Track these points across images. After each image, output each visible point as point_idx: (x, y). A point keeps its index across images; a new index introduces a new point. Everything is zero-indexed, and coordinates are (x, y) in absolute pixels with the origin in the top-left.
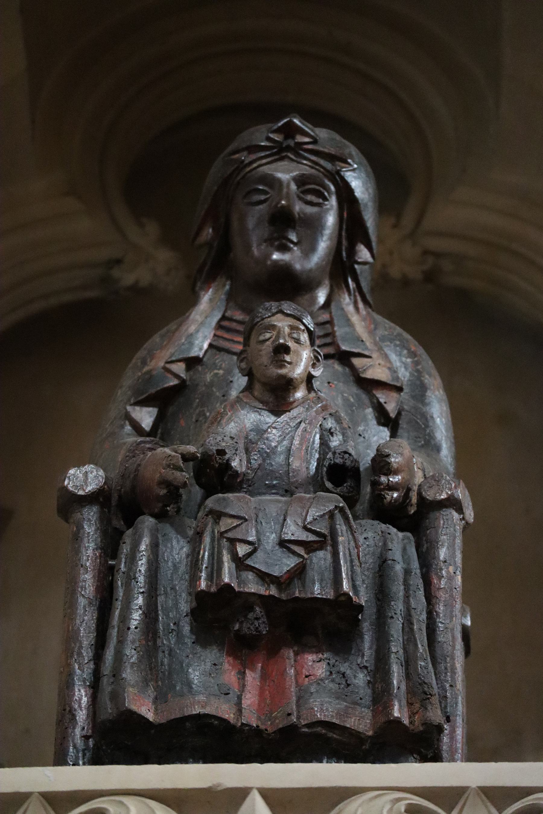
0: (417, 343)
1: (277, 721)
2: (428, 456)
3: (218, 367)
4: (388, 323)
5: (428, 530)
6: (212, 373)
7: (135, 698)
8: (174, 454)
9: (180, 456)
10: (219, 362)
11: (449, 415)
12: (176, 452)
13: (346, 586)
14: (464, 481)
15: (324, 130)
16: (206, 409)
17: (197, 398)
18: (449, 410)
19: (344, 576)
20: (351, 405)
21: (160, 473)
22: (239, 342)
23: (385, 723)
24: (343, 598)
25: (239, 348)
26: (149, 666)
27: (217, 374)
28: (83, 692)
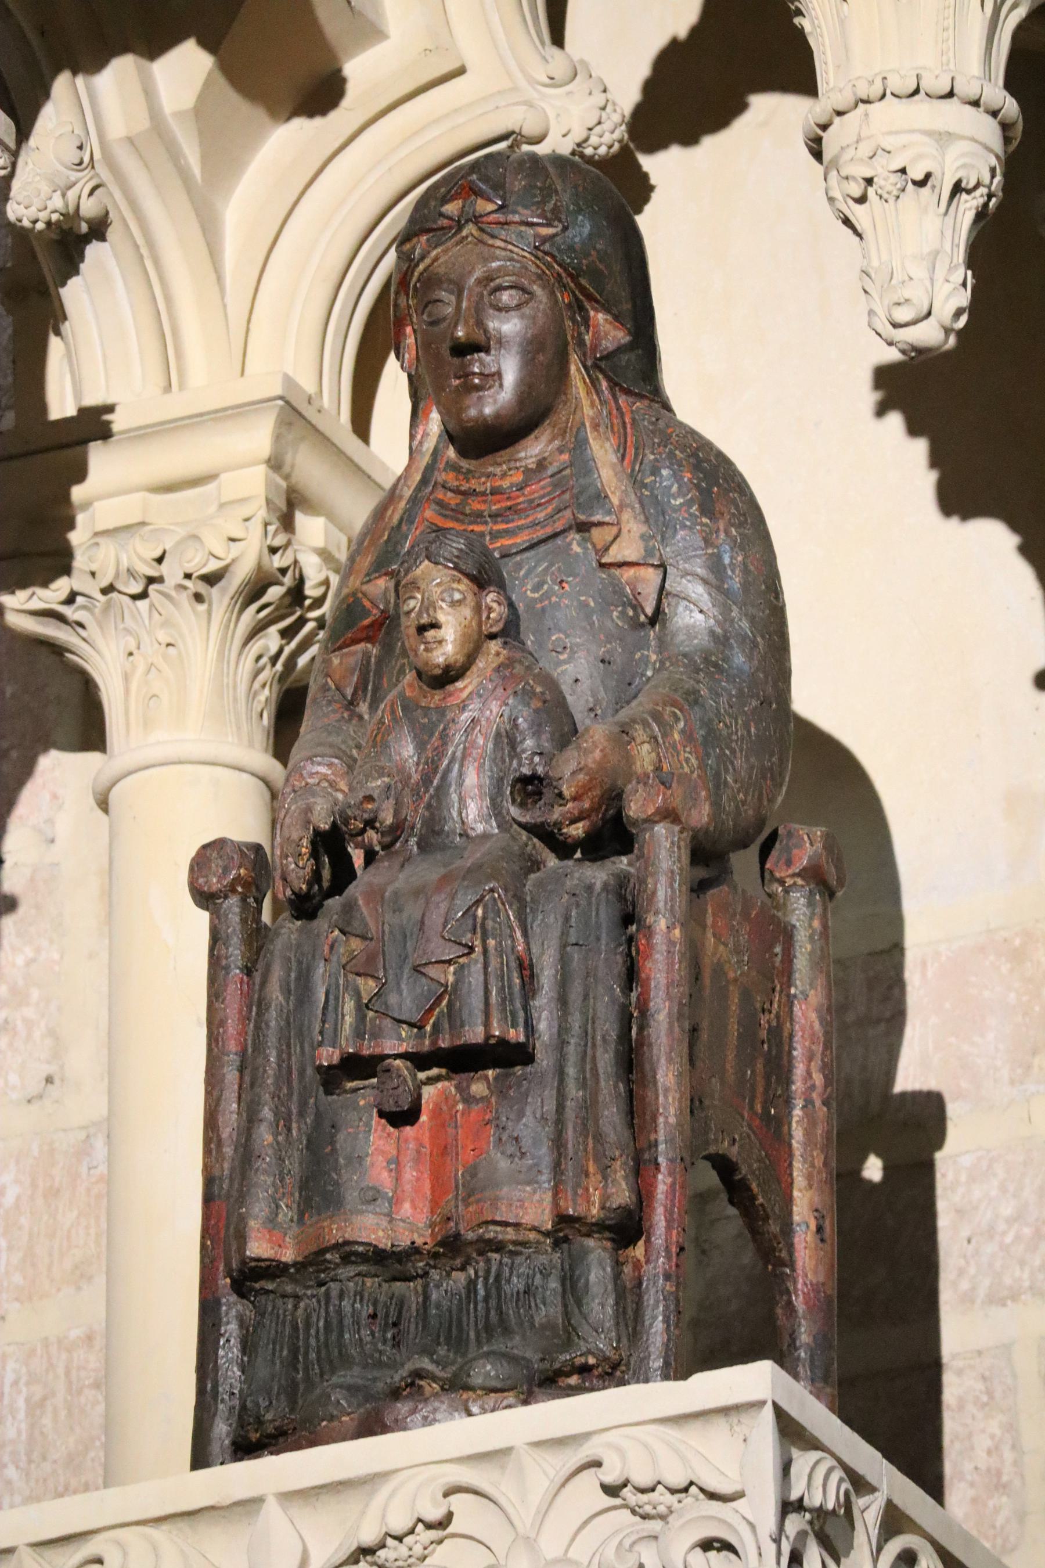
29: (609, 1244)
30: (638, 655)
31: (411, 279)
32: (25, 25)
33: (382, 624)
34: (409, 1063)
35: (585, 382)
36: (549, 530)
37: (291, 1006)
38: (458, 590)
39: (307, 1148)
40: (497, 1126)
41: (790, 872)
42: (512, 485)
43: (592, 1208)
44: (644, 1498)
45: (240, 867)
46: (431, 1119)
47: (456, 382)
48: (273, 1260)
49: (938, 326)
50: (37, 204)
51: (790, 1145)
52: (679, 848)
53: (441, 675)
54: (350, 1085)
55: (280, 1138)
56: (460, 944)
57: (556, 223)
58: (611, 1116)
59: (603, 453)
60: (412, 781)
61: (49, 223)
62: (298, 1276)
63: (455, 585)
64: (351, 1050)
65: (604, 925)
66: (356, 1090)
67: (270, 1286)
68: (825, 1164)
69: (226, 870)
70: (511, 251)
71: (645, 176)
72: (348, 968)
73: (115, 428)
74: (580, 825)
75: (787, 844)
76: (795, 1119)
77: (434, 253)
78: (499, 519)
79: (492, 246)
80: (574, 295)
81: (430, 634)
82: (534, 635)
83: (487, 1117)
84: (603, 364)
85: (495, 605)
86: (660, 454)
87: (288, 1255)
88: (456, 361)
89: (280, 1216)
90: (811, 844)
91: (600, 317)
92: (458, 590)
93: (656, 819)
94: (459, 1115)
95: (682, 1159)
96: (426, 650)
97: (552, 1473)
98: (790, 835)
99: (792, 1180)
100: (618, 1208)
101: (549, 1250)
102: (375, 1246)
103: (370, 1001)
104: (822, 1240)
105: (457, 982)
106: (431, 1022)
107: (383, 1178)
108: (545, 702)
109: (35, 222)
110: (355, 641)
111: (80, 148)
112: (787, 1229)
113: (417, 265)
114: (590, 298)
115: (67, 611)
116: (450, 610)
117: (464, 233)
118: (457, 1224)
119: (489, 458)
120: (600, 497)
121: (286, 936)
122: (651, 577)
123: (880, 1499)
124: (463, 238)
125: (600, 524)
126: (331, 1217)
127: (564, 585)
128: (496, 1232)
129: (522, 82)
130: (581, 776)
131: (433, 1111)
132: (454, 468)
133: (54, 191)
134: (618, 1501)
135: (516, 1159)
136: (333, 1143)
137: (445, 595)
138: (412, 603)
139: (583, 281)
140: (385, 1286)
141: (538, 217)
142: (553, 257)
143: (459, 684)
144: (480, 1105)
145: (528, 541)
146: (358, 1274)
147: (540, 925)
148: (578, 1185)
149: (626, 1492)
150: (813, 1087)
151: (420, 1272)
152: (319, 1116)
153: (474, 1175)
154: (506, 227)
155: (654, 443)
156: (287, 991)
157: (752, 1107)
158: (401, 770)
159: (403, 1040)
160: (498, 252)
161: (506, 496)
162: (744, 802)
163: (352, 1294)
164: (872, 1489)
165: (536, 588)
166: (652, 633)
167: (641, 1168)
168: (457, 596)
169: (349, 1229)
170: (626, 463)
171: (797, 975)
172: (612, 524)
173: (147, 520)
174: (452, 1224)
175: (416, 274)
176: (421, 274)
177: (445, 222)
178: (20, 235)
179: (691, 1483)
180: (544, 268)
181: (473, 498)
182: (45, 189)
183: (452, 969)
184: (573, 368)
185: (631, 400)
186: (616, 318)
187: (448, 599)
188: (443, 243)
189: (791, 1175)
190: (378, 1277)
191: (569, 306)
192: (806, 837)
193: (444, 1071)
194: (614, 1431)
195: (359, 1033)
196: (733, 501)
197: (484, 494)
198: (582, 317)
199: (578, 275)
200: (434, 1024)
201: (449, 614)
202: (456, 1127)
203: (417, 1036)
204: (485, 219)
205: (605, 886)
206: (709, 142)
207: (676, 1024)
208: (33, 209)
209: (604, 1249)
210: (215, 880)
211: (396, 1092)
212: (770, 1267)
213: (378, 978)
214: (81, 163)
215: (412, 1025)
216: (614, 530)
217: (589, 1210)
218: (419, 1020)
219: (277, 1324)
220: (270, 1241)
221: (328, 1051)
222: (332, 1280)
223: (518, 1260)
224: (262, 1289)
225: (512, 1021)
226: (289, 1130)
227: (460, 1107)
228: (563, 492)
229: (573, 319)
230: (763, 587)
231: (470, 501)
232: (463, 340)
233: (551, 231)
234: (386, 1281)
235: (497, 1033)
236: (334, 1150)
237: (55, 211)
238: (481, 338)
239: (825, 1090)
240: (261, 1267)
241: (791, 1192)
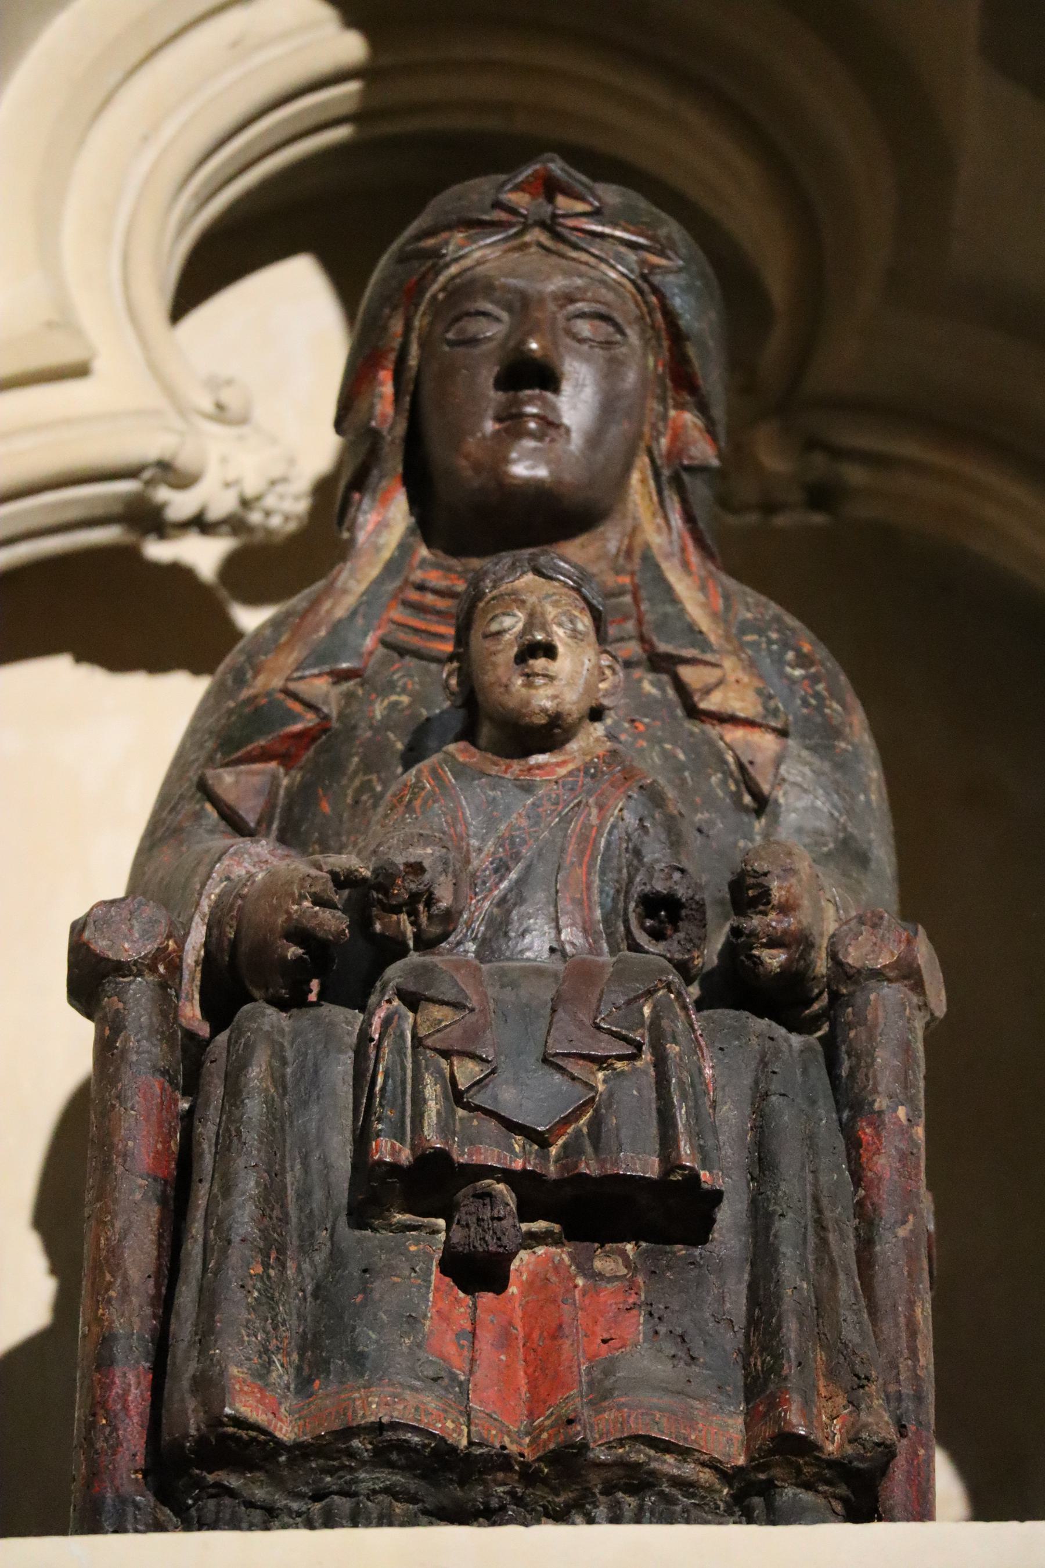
0: (813, 637)
1: (545, 1436)
2: (845, 874)
3: (398, 690)
4: (752, 596)
5: (850, 1029)
6: (386, 702)
7: (246, 1388)
8: (314, 872)
9: (328, 876)
10: (401, 677)
11: (884, 790)
12: (319, 868)
13: (685, 1151)
14: (924, 927)
15: (614, 187)
16: (374, 777)
17: (356, 754)
18: (882, 777)
19: (681, 1128)
20: (680, 768)
21: (288, 912)
22: (441, 637)
23: (772, 1439)
24: (677, 1177)
25: (448, 648)
26: (273, 1320)
27: (396, 703)
28: (132, 1379)
31: (430, 285)
33: (314, 739)
39: (315, 1295)
40: (651, 1314)
53: (543, 726)
54: (399, 1217)
60: (470, 867)
67: (234, 1482)
81: (539, 664)
106: (560, 1142)
110: (264, 756)
117: (527, 238)
127: (637, 724)
131: (531, 1283)
136: (365, 1290)
138: (507, 622)
146: (387, 1491)
151: (494, 1503)
152: (337, 1258)
153: (607, 1373)
176: (453, 278)
193: (556, 1228)
200: (565, 1146)
222: (342, 1493)
226: (284, 1266)
232: (538, 355)
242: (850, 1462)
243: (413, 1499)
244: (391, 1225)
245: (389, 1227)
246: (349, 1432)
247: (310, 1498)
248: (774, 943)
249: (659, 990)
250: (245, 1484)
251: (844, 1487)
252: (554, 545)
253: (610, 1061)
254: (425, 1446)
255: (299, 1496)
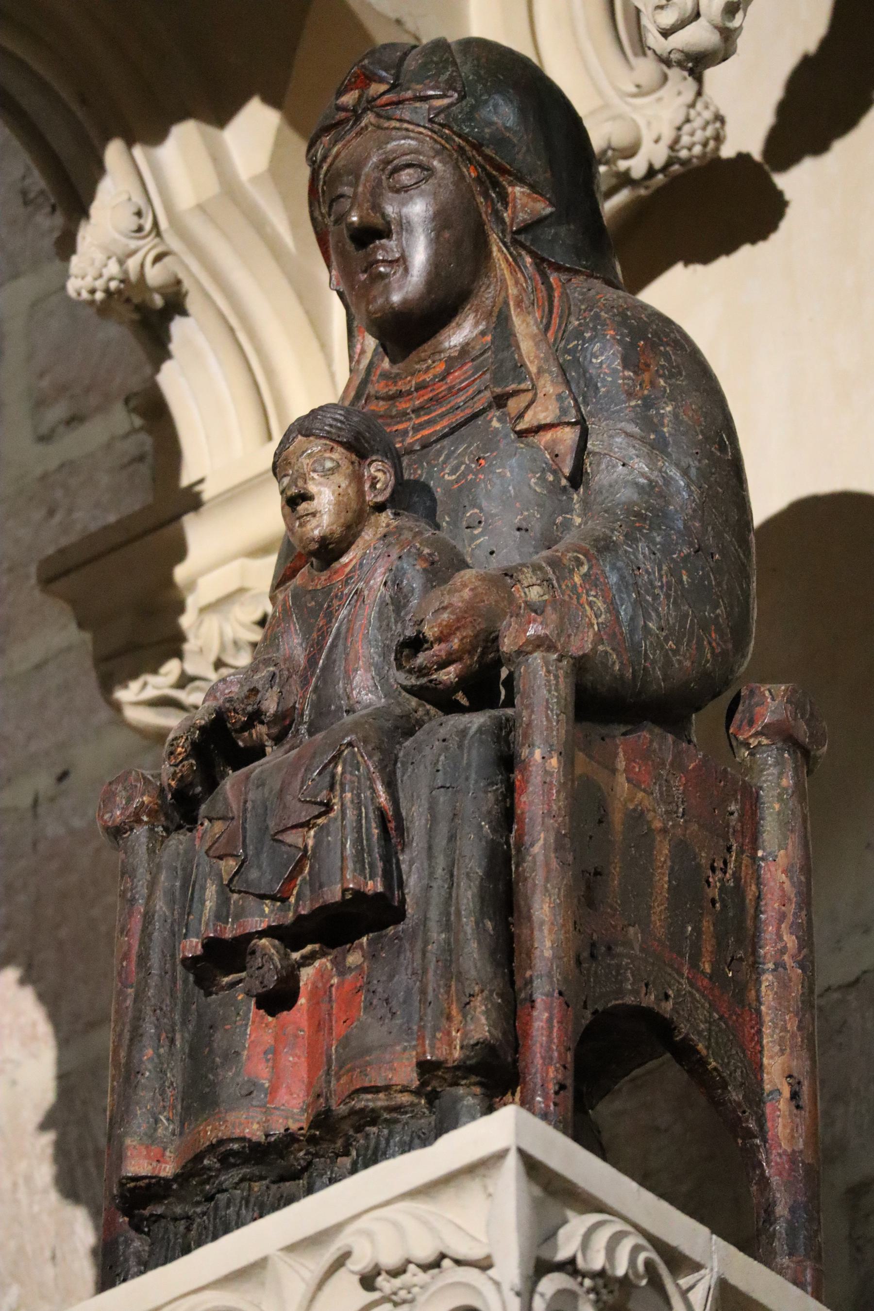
29: (478, 1090)
30: (559, 519)
32: (64, 95)
34: (277, 942)
35: (507, 260)
36: (468, 412)
37: (176, 916)
38: (332, 459)
41: (753, 731)
42: (435, 376)
43: (454, 1051)
44: (397, 1282)
45: (143, 795)
46: (309, 1000)
47: (363, 277)
48: (151, 1177)
49: (710, 28)
50: (92, 273)
51: (759, 1012)
52: (556, 677)
54: (226, 980)
55: (162, 1051)
56: (315, 803)
57: (450, 93)
58: (473, 956)
59: (525, 328)
61: (107, 291)
62: (183, 1193)
63: (327, 455)
64: (212, 935)
65: (474, 764)
66: (233, 985)
67: (159, 1210)
68: (800, 1028)
69: (130, 799)
70: (407, 130)
71: (780, 194)
72: (211, 853)
73: (206, 496)
74: (451, 668)
75: (749, 703)
76: (765, 984)
77: (335, 149)
78: (422, 413)
79: (387, 128)
80: (484, 169)
81: (303, 507)
82: (449, 516)
83: (359, 985)
84: (522, 238)
85: (380, 475)
86: (585, 318)
87: (168, 1170)
88: (361, 253)
89: (160, 1130)
90: (773, 699)
91: (517, 191)
92: (332, 459)
93: (530, 648)
94: (334, 989)
95: (560, 993)
96: (301, 525)
97: (307, 1275)
98: (752, 693)
99: (762, 1047)
100: (477, 1044)
101: (427, 1112)
102: (250, 1140)
103: (231, 880)
104: (798, 1107)
105: (315, 847)
106: (295, 892)
107: (262, 1072)
108: (433, 563)
109: (93, 291)
111: (139, 214)
112: (756, 1097)
113: (320, 167)
114: (503, 171)
115: (181, 695)
116: (322, 479)
118: (327, 1100)
119: (413, 356)
120: (518, 369)
121: (174, 847)
122: (568, 436)
123: (708, 1277)
124: (362, 129)
125: (516, 393)
126: (206, 1120)
127: (482, 461)
128: (368, 1100)
129: (611, 94)
130: (445, 616)
132: (385, 376)
133: (109, 258)
134: (376, 1295)
135: (387, 1021)
136: (210, 1044)
137: (316, 465)
139: (488, 151)
140: (274, 1187)
141: (432, 89)
142: (451, 129)
143: (345, 560)
144: (353, 973)
145: (448, 426)
146: (242, 1180)
147: (410, 777)
148: (436, 1028)
149: (381, 1281)
150: (783, 951)
154: (401, 106)
155: (580, 310)
156: (171, 902)
157: (694, 964)
158: (289, 659)
159: (266, 916)
160: (394, 133)
161: (429, 389)
162: (676, 652)
163: (238, 1201)
164: (697, 1267)
165: (453, 472)
166: (575, 496)
167: (512, 1006)
168: (329, 464)
169: (223, 1128)
170: (550, 334)
171: (765, 836)
172: (528, 390)
173: (247, 585)
174: (322, 1100)
175: (322, 176)
177: (342, 115)
178: (73, 305)
179: (443, 1256)
180: (443, 142)
181: (402, 400)
182: (100, 257)
183: (312, 833)
184: (495, 249)
185: (564, 277)
186: (533, 187)
187: (320, 468)
188: (343, 137)
189: (760, 1042)
190: (265, 1178)
191: (478, 179)
192: (767, 693)
193: (317, 946)
194: (366, 1217)
195: (221, 916)
196: (666, 355)
197: (409, 393)
198: (498, 194)
199: (481, 145)
201: (320, 484)
202: (330, 1001)
203: (280, 909)
204: (379, 102)
205: (480, 730)
206: (840, 147)
207: (553, 855)
208: (89, 279)
209: (475, 1095)
210: (118, 813)
211: (261, 971)
212: (740, 1141)
213: (237, 856)
214: (140, 229)
215: (273, 898)
216: (529, 396)
217: (451, 1054)
218: (279, 891)
219: (167, 1250)
220: (148, 1157)
221: (191, 942)
223: (399, 1127)
224: (152, 1215)
225: (370, 872)
226: (172, 1041)
227: (335, 981)
228: (484, 373)
229: (487, 196)
230: (700, 437)
231: (397, 404)
233: (446, 101)
234: (274, 1182)
235: (351, 886)
236: (211, 1051)
237: (111, 279)
238: (378, 221)
239: (800, 952)
240: (141, 1187)
241: (761, 1059)
242: (465, 1063)
243: (261, 1178)
244: (223, 987)
245: (223, 988)
246: (198, 1158)
247: (205, 1201)
248: (443, 665)
249: (343, 751)
250: (166, 1208)
251: (474, 1077)
252: (438, 335)
253: (312, 822)
254: (244, 1148)
255: (198, 1203)
